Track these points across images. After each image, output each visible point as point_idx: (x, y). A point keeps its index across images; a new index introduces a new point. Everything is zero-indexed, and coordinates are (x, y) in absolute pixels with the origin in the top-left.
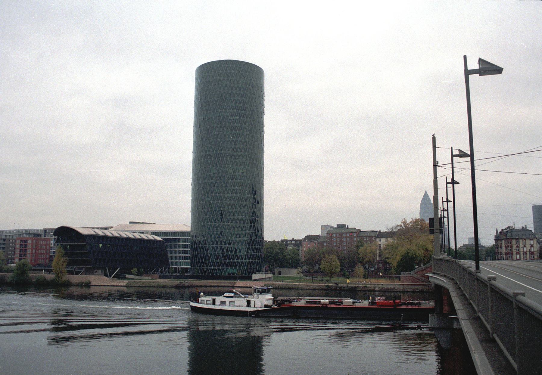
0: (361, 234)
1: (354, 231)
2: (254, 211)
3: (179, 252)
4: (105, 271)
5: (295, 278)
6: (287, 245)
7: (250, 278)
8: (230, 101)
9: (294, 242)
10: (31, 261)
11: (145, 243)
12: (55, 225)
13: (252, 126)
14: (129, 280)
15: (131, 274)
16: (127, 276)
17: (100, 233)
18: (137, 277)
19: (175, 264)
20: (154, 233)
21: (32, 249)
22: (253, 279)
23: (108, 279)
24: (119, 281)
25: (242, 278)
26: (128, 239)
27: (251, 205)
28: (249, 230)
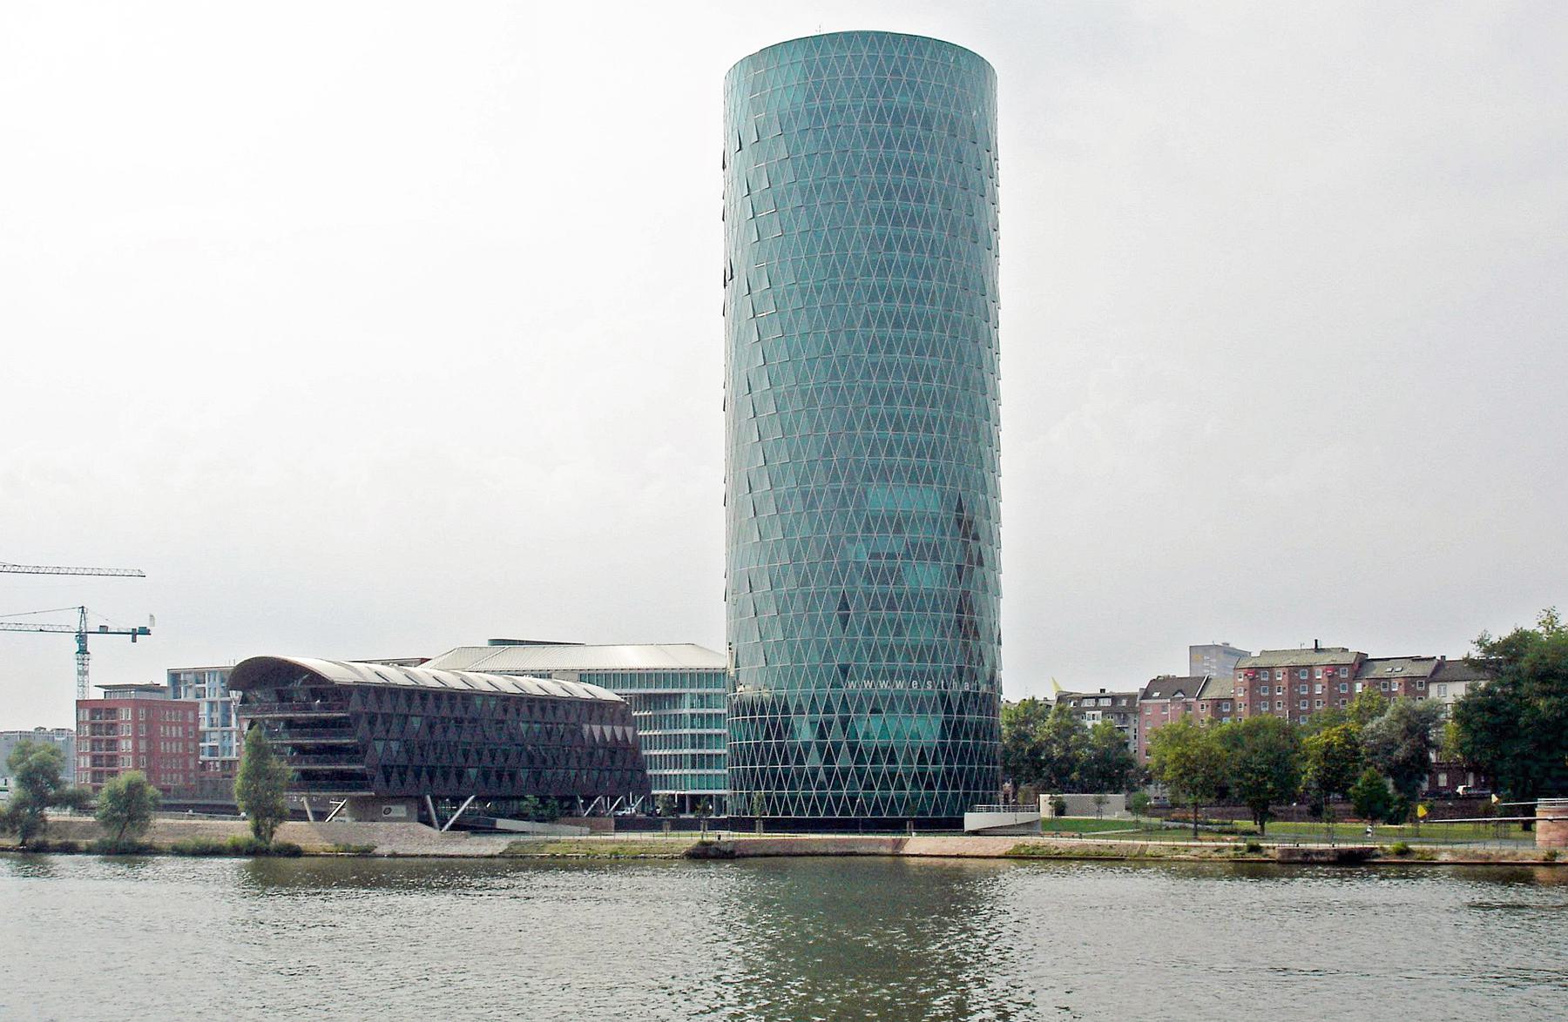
0: (1379, 671)
1: (1340, 659)
2: (966, 594)
3: (678, 741)
5: (1122, 825)
6: (1081, 712)
7: (954, 825)
8: (875, 198)
9: (1106, 703)
10: (186, 779)
11: (459, 705)
12: (232, 658)
13: (952, 179)
14: (514, 838)
15: (520, 816)
16: (501, 823)
17: (397, 677)
18: (539, 826)
19: (664, 782)
20: (586, 676)
21: (136, 739)
22: (968, 827)
23: (436, 833)
24: (477, 839)
25: (928, 826)
27: (954, 571)
28: (953, 585)
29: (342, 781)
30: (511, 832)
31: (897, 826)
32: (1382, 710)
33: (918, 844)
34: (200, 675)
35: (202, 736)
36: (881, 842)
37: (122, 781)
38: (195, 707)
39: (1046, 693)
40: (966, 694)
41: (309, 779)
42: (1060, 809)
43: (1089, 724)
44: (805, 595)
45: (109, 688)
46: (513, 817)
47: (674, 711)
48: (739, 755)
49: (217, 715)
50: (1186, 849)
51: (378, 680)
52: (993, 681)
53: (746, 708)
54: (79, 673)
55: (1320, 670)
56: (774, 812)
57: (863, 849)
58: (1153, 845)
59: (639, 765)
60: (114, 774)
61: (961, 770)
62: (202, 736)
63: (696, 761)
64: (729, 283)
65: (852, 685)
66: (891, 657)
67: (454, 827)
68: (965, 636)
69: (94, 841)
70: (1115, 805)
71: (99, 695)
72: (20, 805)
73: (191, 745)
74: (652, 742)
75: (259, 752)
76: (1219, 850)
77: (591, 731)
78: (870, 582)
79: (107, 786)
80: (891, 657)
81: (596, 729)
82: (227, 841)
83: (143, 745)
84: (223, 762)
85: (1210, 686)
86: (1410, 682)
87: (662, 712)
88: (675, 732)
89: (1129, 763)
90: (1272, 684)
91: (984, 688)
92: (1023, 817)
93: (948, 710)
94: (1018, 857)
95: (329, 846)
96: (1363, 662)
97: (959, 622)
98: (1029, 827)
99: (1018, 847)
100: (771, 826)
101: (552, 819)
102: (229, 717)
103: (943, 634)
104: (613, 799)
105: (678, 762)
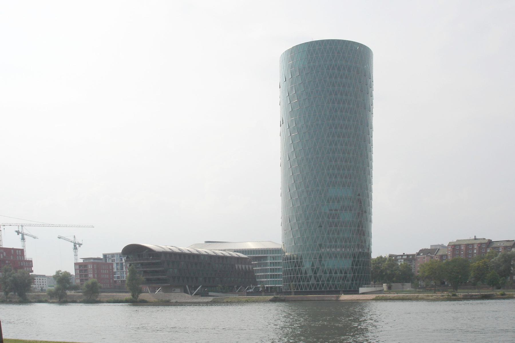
1: (483, 242)
2: (361, 221)
3: (266, 271)
4: (185, 287)
7: (356, 292)
8: (331, 88)
9: (405, 257)
16: (210, 294)
18: (222, 294)
20: (236, 251)
24: (203, 298)
25: (347, 292)
26: (232, 258)
29: (159, 281)
30: (213, 296)
31: (338, 292)
32: (496, 255)
33: (344, 297)
34: (113, 255)
35: (115, 273)
36: (333, 297)
37: (90, 282)
38: (112, 264)
39: (385, 254)
40: (360, 252)
41: (149, 281)
42: (389, 288)
43: (399, 264)
44: (307, 223)
45: (85, 259)
46: (214, 292)
47: (264, 262)
48: (285, 273)
49: (119, 267)
50: (432, 296)
51: (170, 251)
52: (369, 248)
53: (287, 258)
54: (75, 255)
55: (476, 245)
56: (297, 289)
57: (327, 299)
58: (421, 295)
59: (255, 278)
60: (87, 280)
61: (358, 276)
62: (115, 273)
63: (272, 276)
64: (282, 125)
65: (323, 250)
66: (336, 241)
67: (195, 294)
68: (360, 235)
69: (82, 300)
70: (408, 286)
71: (81, 261)
72: (58, 289)
73: (111, 276)
74: (258, 271)
75: (133, 272)
76: (443, 296)
77: (238, 267)
78: (329, 218)
79: (85, 283)
80: (336, 241)
81: (240, 266)
82: (124, 299)
83: (96, 276)
84: (121, 281)
85: (440, 251)
86: (505, 248)
87: (261, 262)
88: (265, 268)
89: (412, 275)
90: (460, 249)
91: (366, 251)
92: (378, 289)
93: (354, 257)
94: (376, 299)
95: (156, 300)
96: (490, 242)
97: (358, 230)
98: (381, 292)
99: (376, 297)
100: (296, 293)
101: (226, 292)
102: (123, 268)
103: (353, 234)
104: (245, 288)
105: (266, 277)
